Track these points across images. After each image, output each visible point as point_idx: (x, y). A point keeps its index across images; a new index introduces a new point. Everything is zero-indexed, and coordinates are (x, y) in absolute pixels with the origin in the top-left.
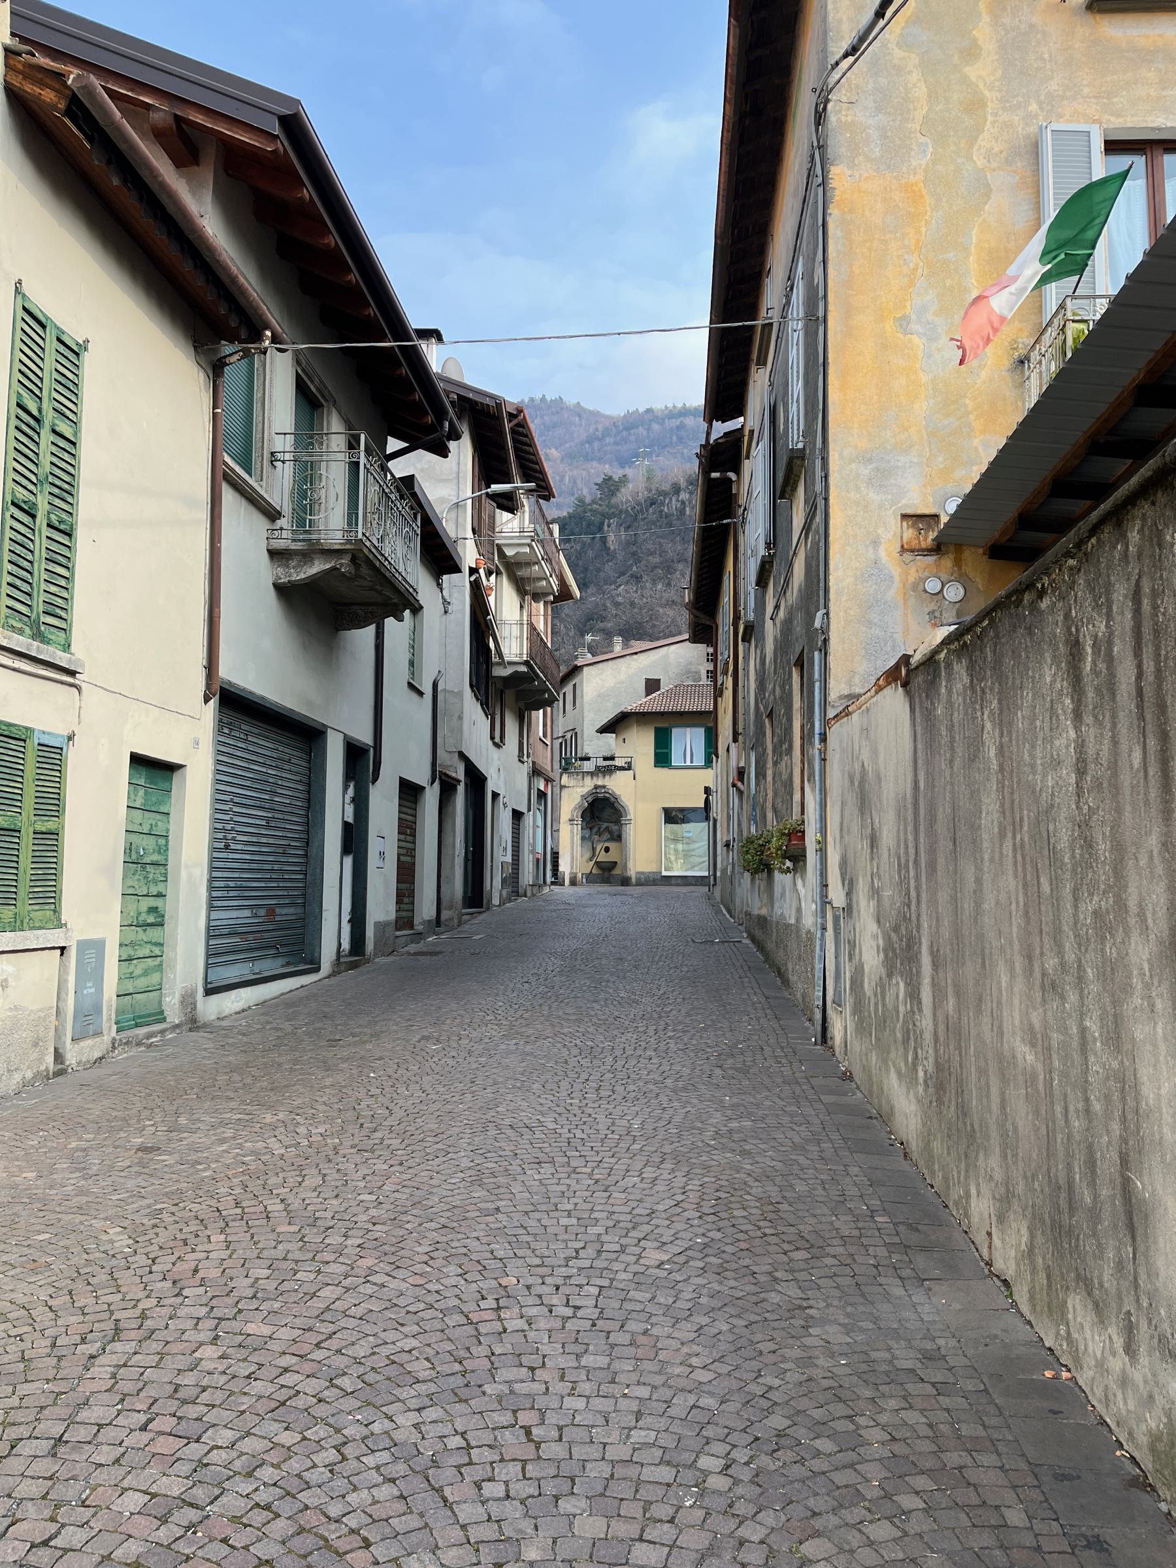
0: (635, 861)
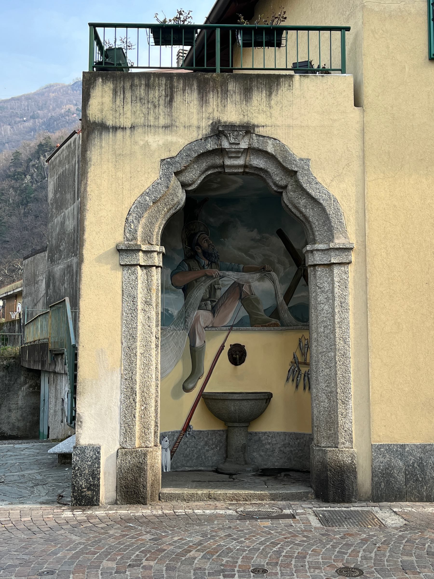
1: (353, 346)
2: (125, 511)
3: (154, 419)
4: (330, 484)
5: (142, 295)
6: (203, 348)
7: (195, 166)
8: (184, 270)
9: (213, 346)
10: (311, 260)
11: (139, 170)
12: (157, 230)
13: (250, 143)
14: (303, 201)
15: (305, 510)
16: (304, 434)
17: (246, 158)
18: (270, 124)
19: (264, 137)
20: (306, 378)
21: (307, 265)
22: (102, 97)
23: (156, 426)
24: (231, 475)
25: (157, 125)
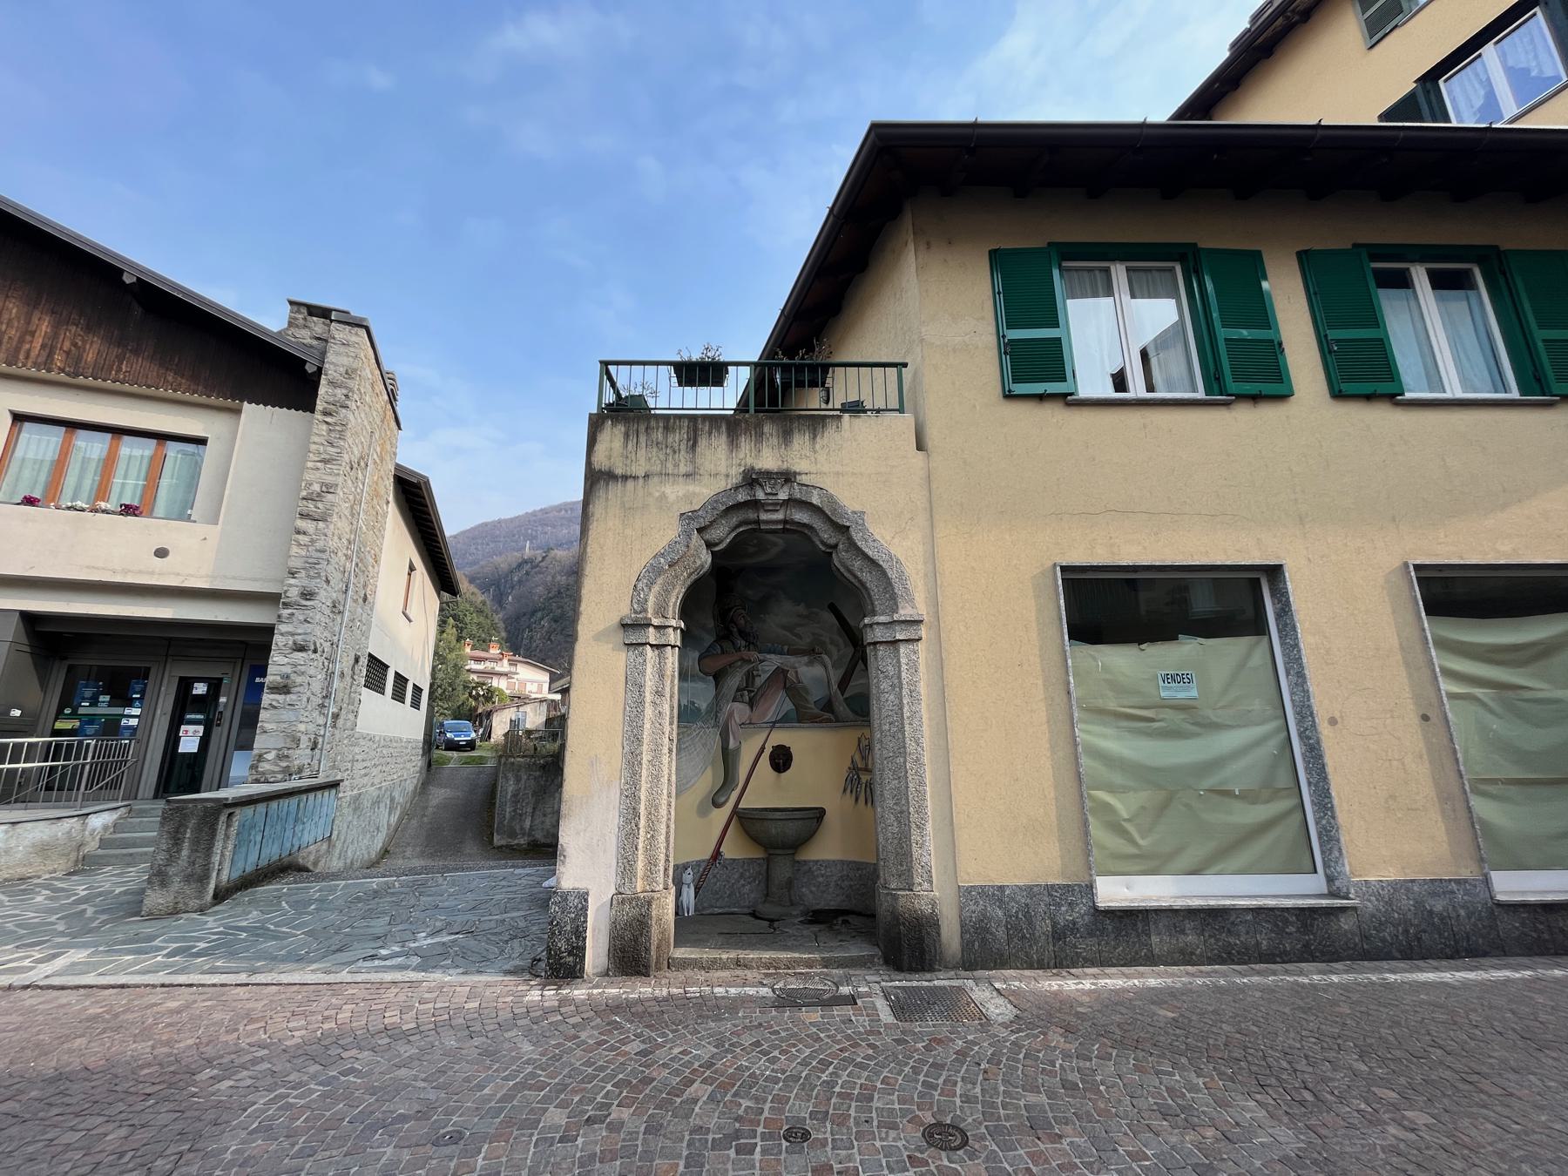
2: (615, 991)
4: (905, 945)
6: (738, 750)
9: (749, 748)
10: (870, 637)
23: (667, 860)
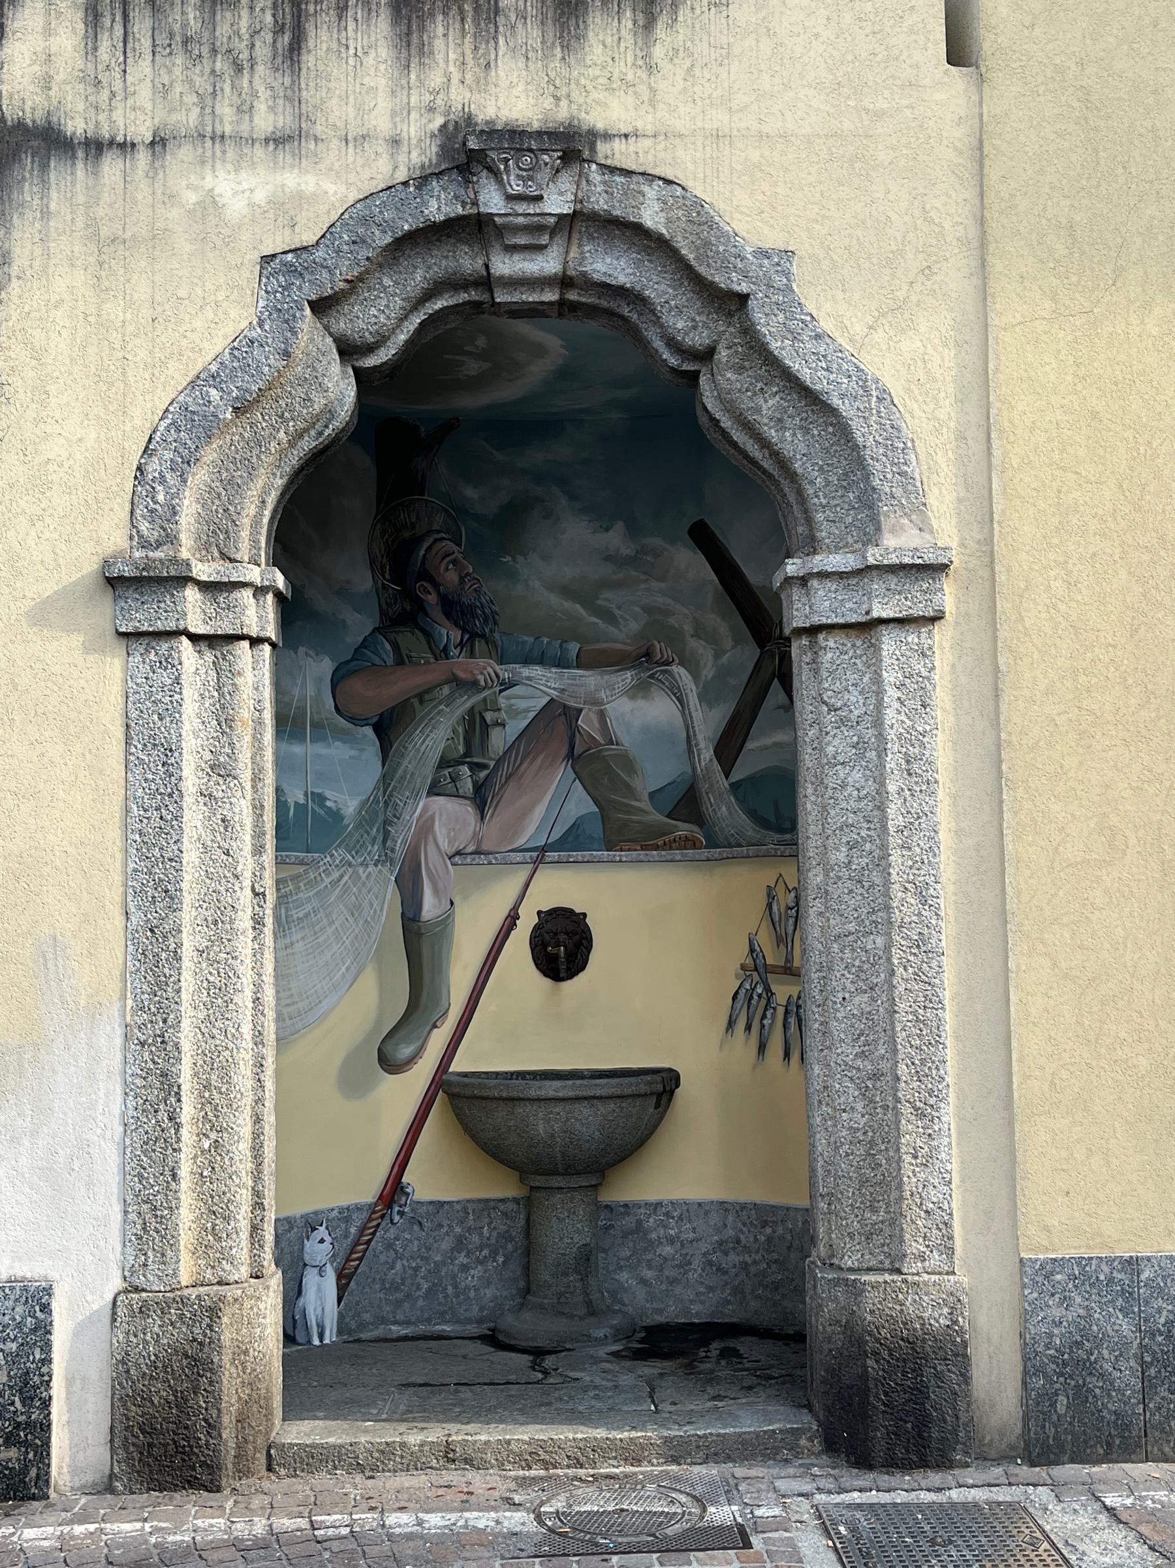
0: (1002, 1107)
1: (950, 912)
2: (135, 1525)
3: (250, 1183)
5: (199, 741)
6: (445, 922)
7: (387, 281)
8: (377, 661)
9: (479, 914)
10: (800, 612)
11: (182, 293)
12: (252, 510)
13: (580, 195)
14: (771, 403)
15: (785, 1506)
16: (788, 1209)
17: (567, 252)
18: (649, 127)
19: (628, 173)
20: (792, 1020)
21: (787, 631)
22: (48, 32)
23: (258, 1205)
24: (538, 1353)
25: (245, 135)
